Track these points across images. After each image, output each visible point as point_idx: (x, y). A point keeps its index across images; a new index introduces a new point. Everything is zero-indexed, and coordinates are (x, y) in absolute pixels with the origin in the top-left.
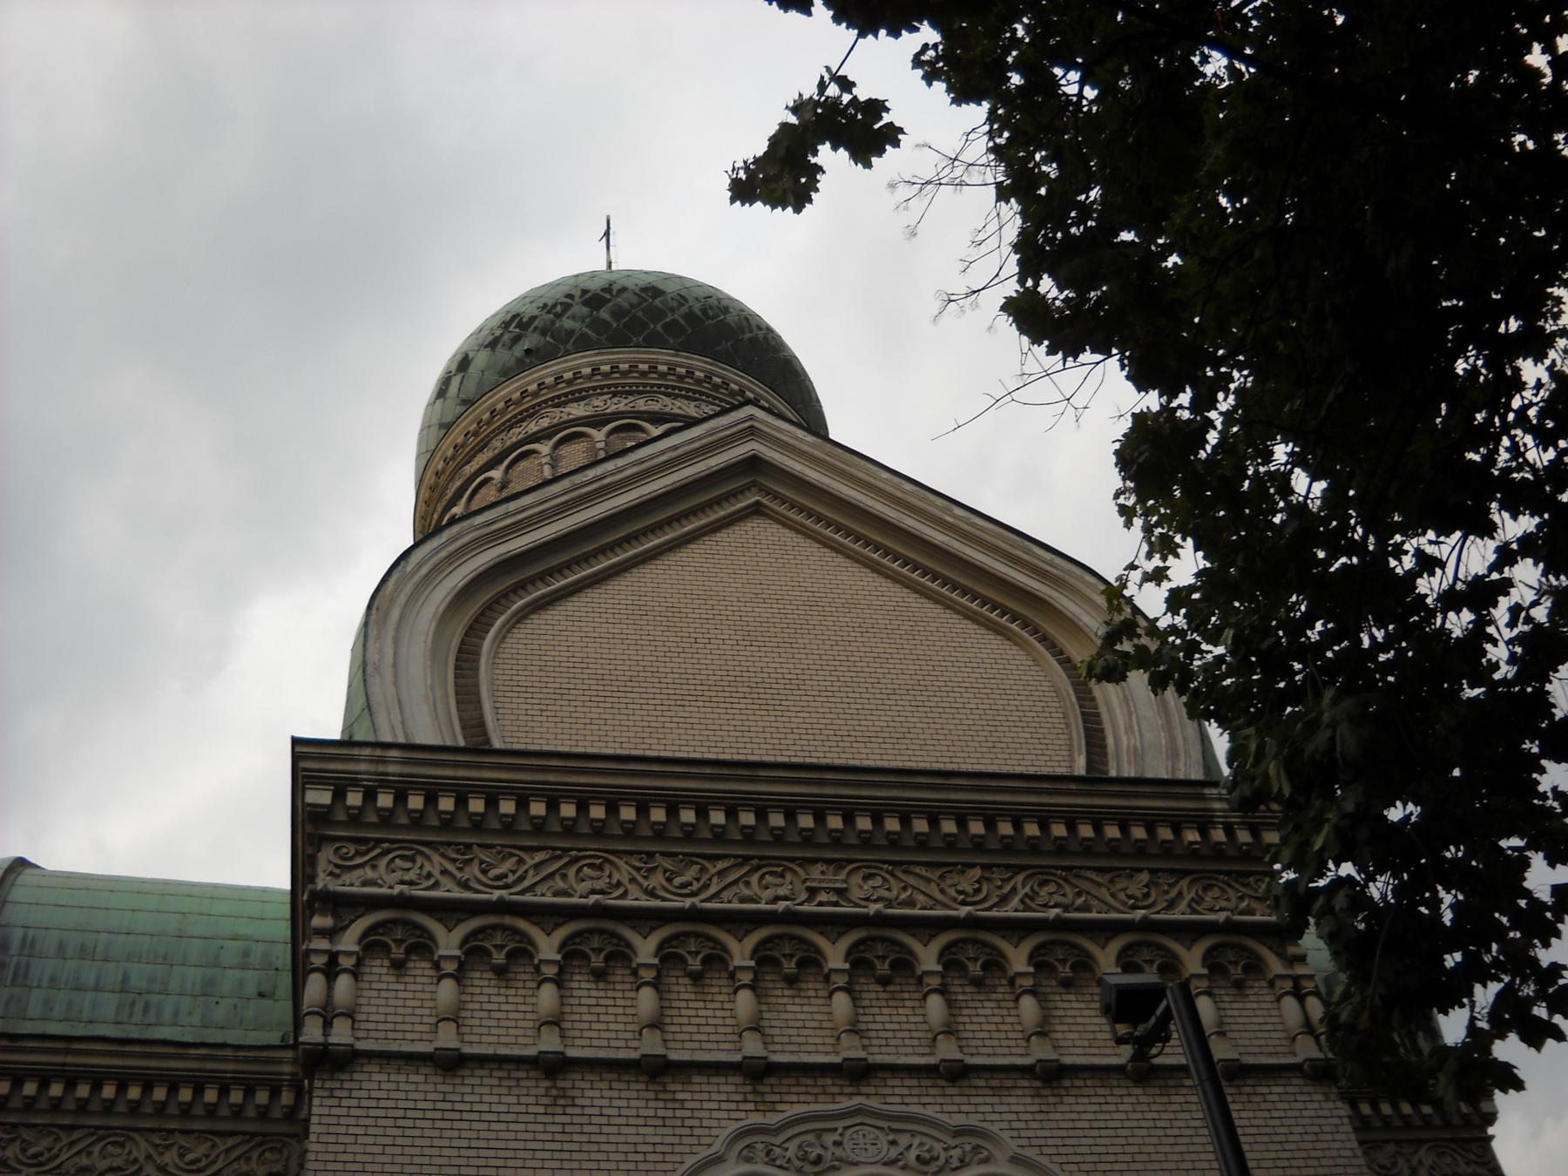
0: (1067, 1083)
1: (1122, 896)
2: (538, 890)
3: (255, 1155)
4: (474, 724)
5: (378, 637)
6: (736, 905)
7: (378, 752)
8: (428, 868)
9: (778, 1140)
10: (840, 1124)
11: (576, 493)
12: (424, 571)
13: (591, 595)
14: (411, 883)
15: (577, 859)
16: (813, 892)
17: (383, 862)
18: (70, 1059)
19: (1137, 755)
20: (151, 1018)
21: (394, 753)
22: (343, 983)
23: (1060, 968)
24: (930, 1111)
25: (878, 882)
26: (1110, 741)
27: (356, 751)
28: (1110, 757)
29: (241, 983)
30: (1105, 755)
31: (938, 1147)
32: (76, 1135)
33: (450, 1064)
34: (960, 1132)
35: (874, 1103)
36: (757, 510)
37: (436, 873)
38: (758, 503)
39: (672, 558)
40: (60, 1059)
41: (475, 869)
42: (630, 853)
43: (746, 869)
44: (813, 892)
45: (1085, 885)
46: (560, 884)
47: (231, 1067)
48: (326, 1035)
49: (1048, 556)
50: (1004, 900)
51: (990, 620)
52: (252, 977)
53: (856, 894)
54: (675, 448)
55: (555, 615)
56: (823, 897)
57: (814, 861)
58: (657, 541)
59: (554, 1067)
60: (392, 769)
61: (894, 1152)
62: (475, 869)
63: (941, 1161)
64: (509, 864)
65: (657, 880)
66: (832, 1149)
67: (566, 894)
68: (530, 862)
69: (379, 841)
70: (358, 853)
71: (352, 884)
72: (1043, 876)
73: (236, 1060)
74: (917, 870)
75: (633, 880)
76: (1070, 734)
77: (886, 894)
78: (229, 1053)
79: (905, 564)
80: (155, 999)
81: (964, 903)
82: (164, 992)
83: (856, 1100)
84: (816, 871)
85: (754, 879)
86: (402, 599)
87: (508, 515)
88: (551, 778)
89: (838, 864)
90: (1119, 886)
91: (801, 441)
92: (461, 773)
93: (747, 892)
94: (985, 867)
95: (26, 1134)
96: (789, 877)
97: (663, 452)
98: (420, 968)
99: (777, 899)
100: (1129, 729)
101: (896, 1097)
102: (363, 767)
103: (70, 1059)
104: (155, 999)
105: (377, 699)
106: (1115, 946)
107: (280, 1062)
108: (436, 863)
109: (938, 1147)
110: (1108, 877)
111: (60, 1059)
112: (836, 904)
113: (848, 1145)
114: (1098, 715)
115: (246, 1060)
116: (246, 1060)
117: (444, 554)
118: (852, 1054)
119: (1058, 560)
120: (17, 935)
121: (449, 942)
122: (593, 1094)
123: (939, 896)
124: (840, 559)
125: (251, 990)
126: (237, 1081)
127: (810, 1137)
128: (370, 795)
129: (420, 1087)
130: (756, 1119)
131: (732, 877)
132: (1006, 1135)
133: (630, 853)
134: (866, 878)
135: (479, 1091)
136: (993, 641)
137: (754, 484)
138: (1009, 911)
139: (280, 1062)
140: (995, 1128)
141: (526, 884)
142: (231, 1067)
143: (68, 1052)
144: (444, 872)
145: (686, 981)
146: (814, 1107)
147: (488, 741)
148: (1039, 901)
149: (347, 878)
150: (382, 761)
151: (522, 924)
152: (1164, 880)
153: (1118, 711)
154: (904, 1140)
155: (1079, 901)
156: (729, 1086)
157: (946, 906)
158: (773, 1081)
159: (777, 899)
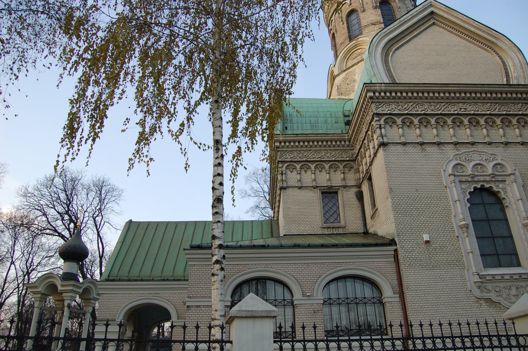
0: (509, 145)
1: (516, 109)
2: (412, 110)
3: (343, 154)
4: (391, 76)
5: (372, 60)
6: (447, 112)
7: (380, 85)
8: (392, 107)
9: (461, 156)
10: (471, 153)
11: (400, 23)
12: (376, 44)
13: (406, 46)
14: (390, 110)
15: (418, 104)
16: (460, 109)
17: (384, 106)
18: (308, 138)
19: (517, 78)
20: (317, 128)
21: (383, 85)
22: (383, 130)
23: (506, 123)
24: (486, 151)
25: (471, 106)
26: (510, 74)
27: (376, 85)
28: (510, 78)
29: (332, 120)
30: (509, 78)
31: (488, 157)
32: (311, 151)
33: (404, 144)
34: (492, 154)
35: (476, 149)
36: (434, 24)
37: (394, 108)
38: (434, 22)
39: (419, 36)
40: (306, 138)
41: (400, 107)
42: (427, 102)
43: (416, 104)
44: (460, 109)
45: (509, 106)
46: (416, 109)
47: (336, 138)
48: (383, 140)
49: (496, 33)
50: (495, 109)
51: (484, 48)
52: (333, 119)
53: (469, 109)
54: (417, 11)
55: (400, 51)
56: (463, 110)
57: (460, 103)
58: (416, 33)
59: (422, 144)
60: (383, 88)
61: (481, 158)
62: (400, 107)
63: (489, 160)
64: (406, 106)
65: (433, 108)
66: (470, 158)
67: (417, 111)
68: (410, 105)
69: (383, 102)
70: (284, 153)
71: (380, 111)
72: (502, 104)
73: (337, 136)
74: (478, 104)
75: (428, 108)
76: (502, 73)
77: (474, 109)
78: (336, 135)
79: (477, 42)
80: (317, 124)
81: (488, 110)
82: (318, 123)
83: (473, 149)
84: (460, 105)
85: (450, 106)
86: (374, 51)
87: (389, 30)
88: (411, 88)
89: (464, 103)
90: (516, 106)
91: (494, 33)
92: (395, 88)
93: (449, 109)
94: (491, 103)
95: (302, 152)
96: (456, 106)
97: (415, 12)
98: (395, 126)
99: (455, 111)
100: (514, 72)
101: (479, 148)
102: (378, 88)
103: (308, 138)
104: (317, 124)
105: (375, 73)
106: (516, 118)
107: (345, 136)
108: (393, 106)
109: (488, 157)
110: (514, 104)
111: (306, 138)
112: (465, 111)
113: (473, 157)
114: (507, 69)
115: (339, 136)
116: (339, 136)
117: (379, 40)
118: (472, 141)
119: (498, 34)
120: (288, 114)
121: (399, 121)
122: (429, 148)
123: (483, 109)
124: (452, 34)
125: (334, 122)
126: (329, 140)
127: (466, 156)
128: (380, 93)
129: (400, 148)
130: (457, 153)
131: (446, 106)
132: (499, 155)
133: (427, 102)
134: (470, 106)
135: (409, 148)
136: (485, 52)
137: (432, 17)
138: (496, 112)
139: (345, 136)
140: (497, 154)
141: (410, 109)
142: (336, 138)
143: (307, 136)
144: (395, 108)
145: (440, 127)
146: (466, 150)
147: (396, 81)
148: (501, 110)
149: (379, 110)
150: (381, 86)
151: (411, 117)
152: (524, 105)
153: (511, 68)
154: (482, 156)
155: (509, 110)
156: (451, 146)
157: (484, 111)
158: (458, 145)
159: (455, 111)
